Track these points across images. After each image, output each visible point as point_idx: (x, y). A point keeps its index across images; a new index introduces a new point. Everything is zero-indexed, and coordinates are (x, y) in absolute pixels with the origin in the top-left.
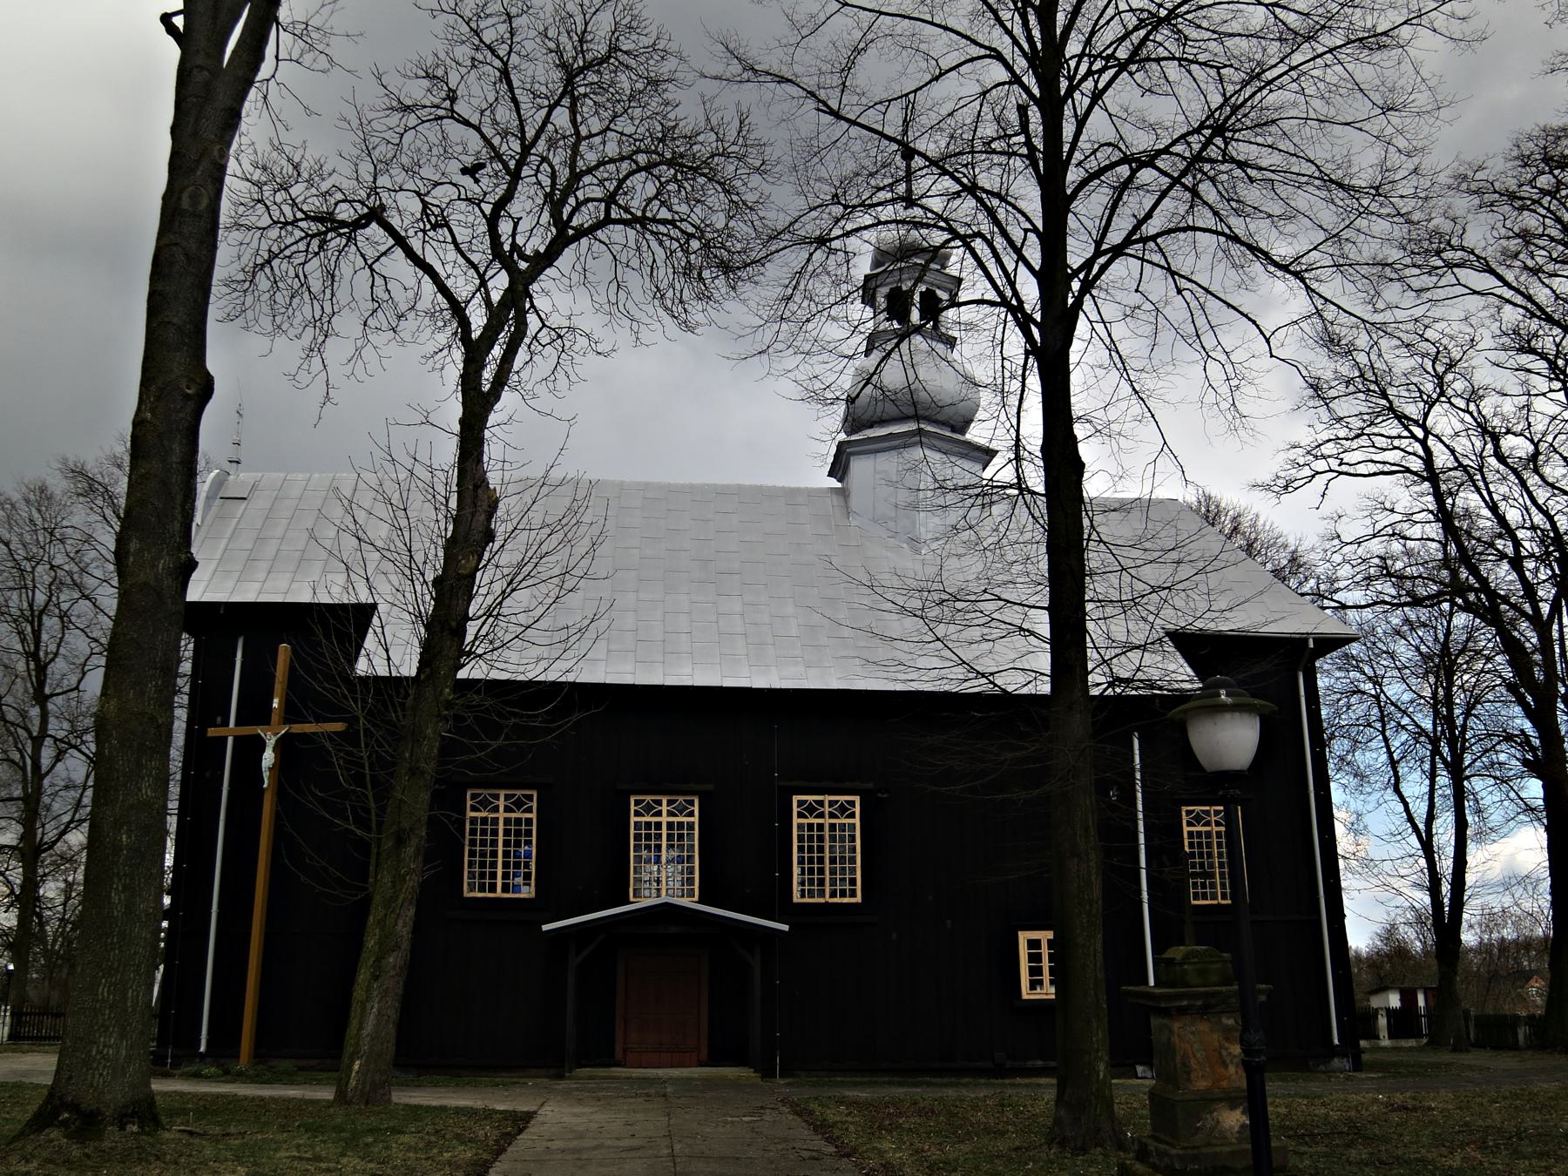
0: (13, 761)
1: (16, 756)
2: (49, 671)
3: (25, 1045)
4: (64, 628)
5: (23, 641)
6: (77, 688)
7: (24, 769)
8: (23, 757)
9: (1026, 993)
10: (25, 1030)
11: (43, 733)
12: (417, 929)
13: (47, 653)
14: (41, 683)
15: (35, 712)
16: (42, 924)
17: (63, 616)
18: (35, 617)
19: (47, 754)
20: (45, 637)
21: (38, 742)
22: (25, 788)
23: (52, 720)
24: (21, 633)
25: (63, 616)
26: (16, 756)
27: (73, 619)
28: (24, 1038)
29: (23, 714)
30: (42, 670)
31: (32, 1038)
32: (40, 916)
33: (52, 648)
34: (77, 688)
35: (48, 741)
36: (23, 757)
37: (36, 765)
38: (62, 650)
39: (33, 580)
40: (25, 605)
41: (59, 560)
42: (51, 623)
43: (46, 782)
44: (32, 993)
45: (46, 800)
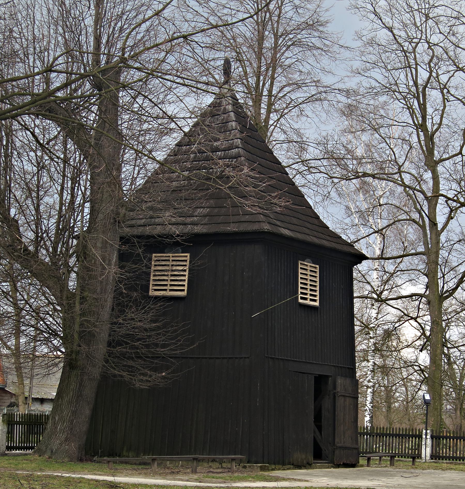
0: (414, 221)
1: (416, 216)
2: (436, 140)
3: (444, 464)
4: (445, 100)
5: (412, 114)
6: (460, 153)
7: (423, 227)
8: (421, 216)
9: (184, 294)
10: (444, 452)
11: (436, 195)
12: (353, 325)
13: (433, 125)
14: (430, 152)
15: (428, 176)
16: (450, 363)
17: (443, 88)
18: (420, 94)
19: (441, 212)
20: (430, 110)
21: (432, 201)
22: (426, 244)
23: (442, 181)
24: (410, 108)
25: (443, 88)
26: (416, 216)
27: (452, 91)
28: (443, 458)
29: (419, 179)
30: (430, 138)
31: (449, 458)
32: (448, 357)
33: (437, 119)
34: (460, 153)
35: (441, 200)
36: (421, 216)
37: (434, 224)
38: (445, 121)
39: (415, 59)
40: (411, 83)
41: (434, 39)
42: (434, 96)
43: (443, 238)
44: (447, 421)
45: (443, 253)
